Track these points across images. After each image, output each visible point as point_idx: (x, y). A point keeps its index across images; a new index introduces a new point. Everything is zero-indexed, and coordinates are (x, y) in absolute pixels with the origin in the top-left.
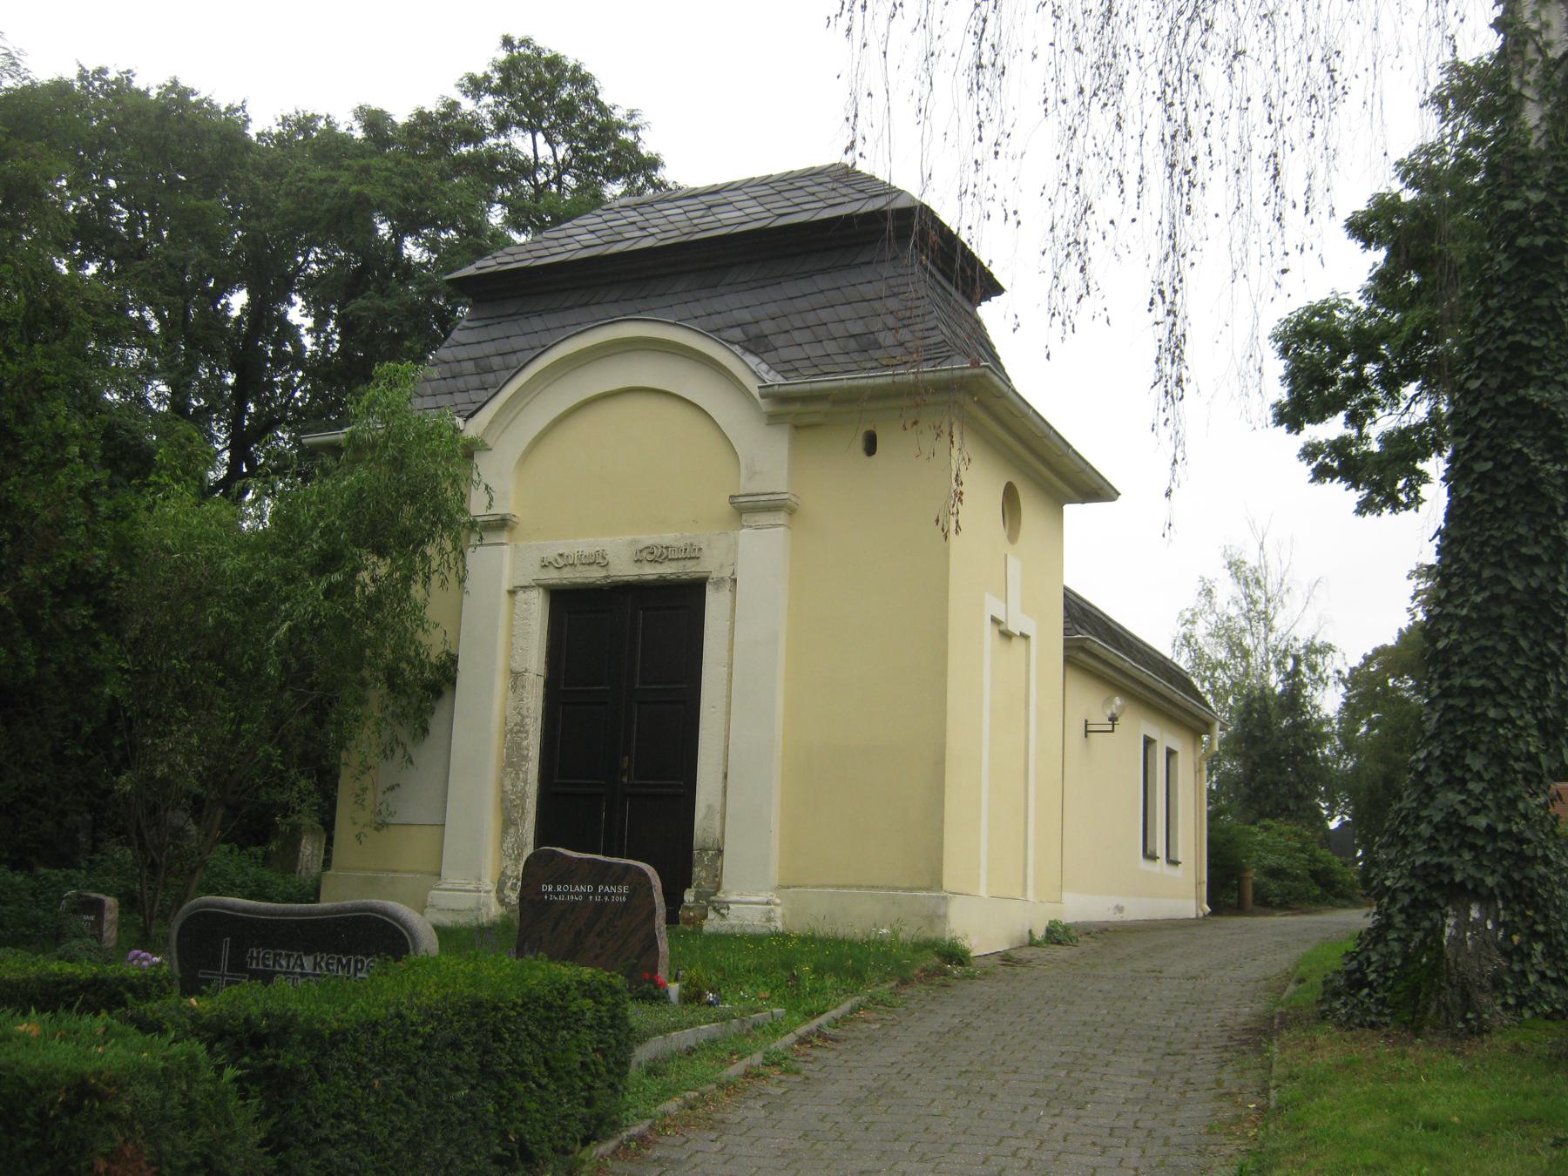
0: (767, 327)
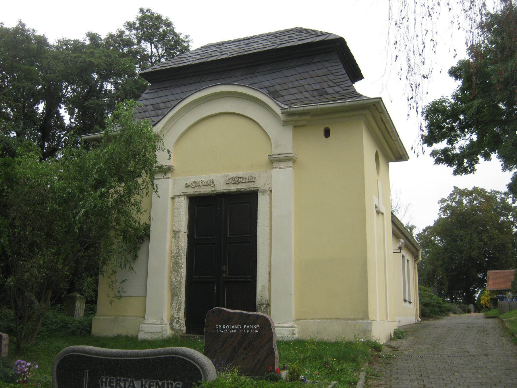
0: (278, 88)
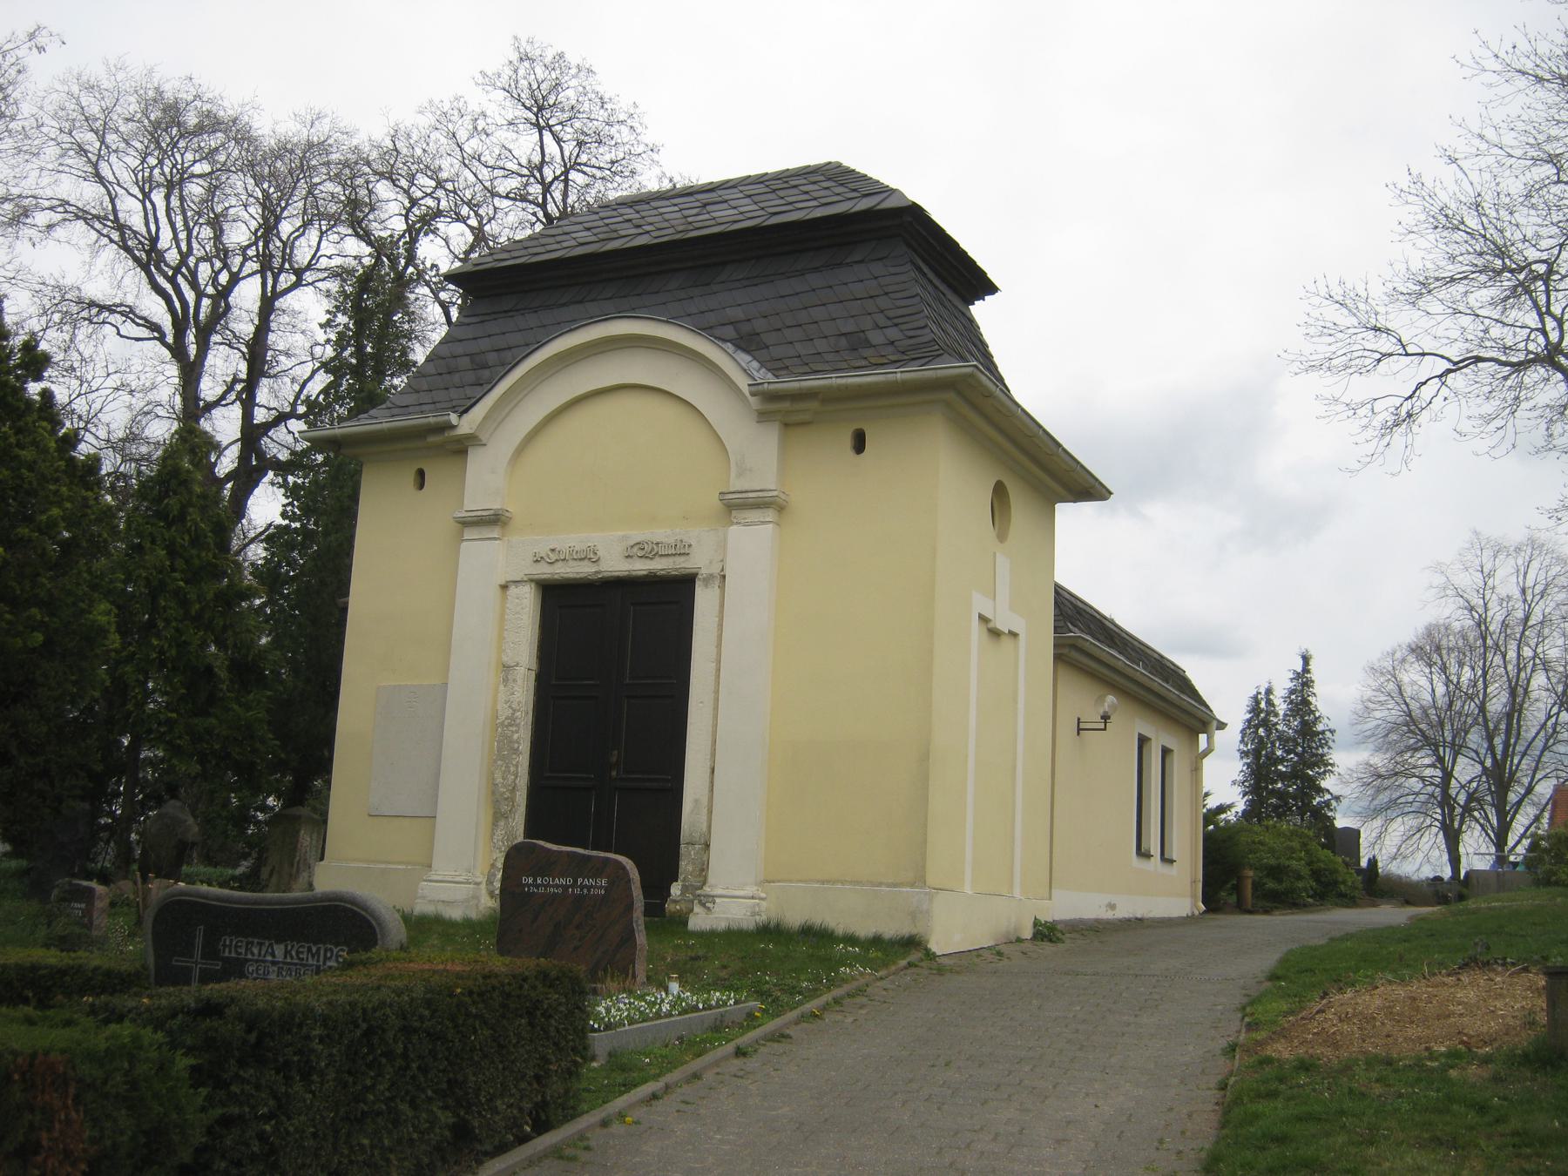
0: (760, 325)
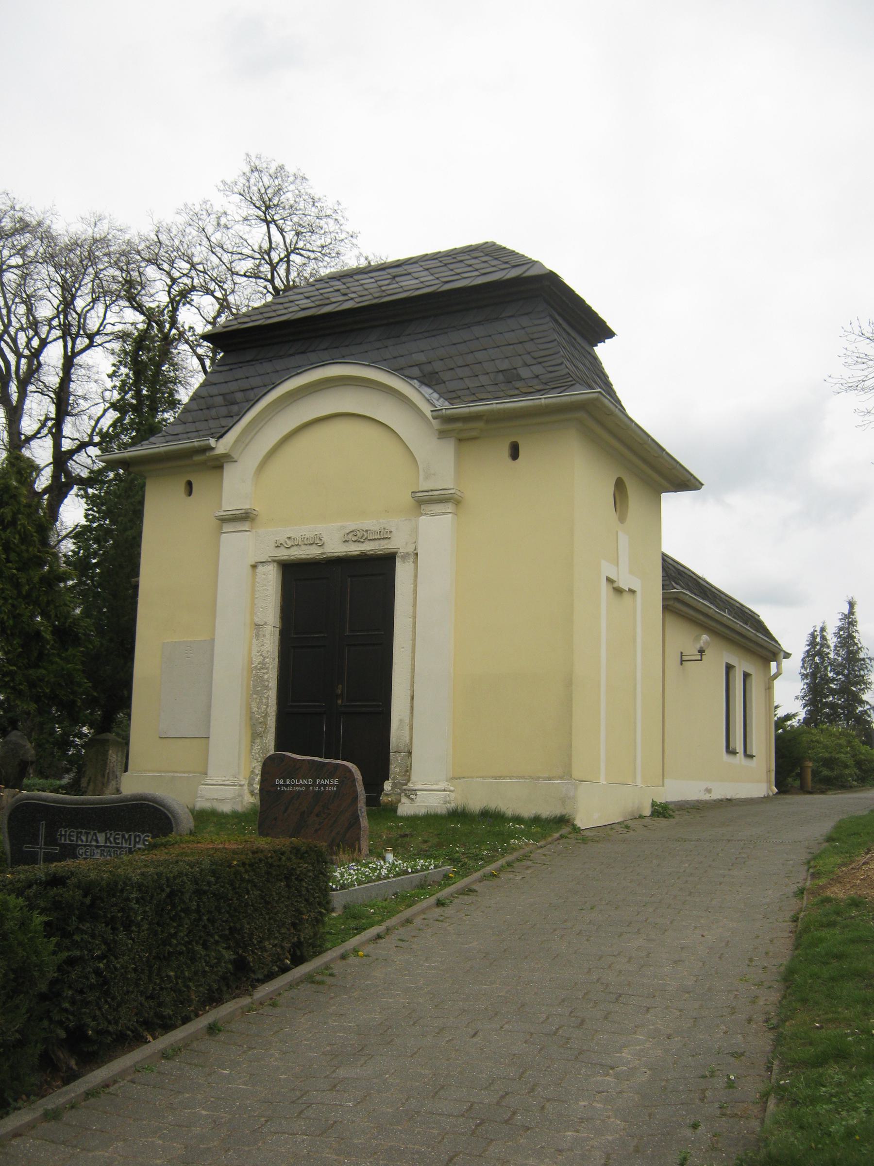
0: (438, 366)
